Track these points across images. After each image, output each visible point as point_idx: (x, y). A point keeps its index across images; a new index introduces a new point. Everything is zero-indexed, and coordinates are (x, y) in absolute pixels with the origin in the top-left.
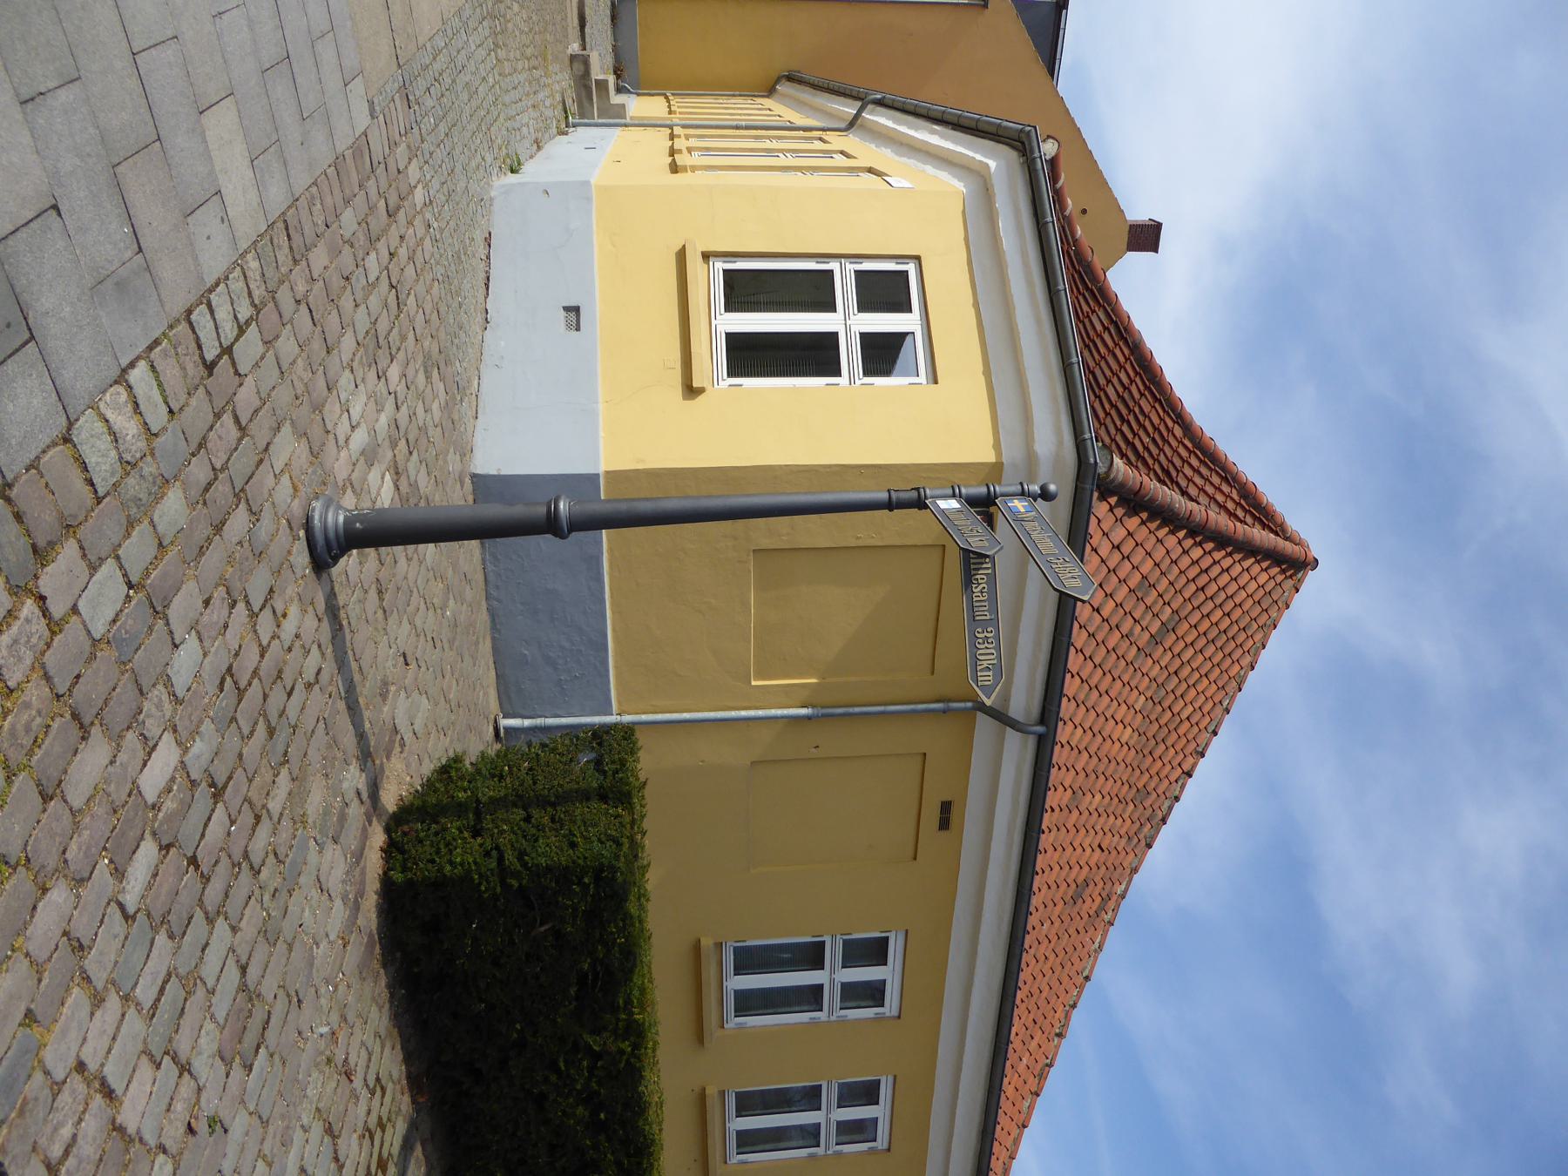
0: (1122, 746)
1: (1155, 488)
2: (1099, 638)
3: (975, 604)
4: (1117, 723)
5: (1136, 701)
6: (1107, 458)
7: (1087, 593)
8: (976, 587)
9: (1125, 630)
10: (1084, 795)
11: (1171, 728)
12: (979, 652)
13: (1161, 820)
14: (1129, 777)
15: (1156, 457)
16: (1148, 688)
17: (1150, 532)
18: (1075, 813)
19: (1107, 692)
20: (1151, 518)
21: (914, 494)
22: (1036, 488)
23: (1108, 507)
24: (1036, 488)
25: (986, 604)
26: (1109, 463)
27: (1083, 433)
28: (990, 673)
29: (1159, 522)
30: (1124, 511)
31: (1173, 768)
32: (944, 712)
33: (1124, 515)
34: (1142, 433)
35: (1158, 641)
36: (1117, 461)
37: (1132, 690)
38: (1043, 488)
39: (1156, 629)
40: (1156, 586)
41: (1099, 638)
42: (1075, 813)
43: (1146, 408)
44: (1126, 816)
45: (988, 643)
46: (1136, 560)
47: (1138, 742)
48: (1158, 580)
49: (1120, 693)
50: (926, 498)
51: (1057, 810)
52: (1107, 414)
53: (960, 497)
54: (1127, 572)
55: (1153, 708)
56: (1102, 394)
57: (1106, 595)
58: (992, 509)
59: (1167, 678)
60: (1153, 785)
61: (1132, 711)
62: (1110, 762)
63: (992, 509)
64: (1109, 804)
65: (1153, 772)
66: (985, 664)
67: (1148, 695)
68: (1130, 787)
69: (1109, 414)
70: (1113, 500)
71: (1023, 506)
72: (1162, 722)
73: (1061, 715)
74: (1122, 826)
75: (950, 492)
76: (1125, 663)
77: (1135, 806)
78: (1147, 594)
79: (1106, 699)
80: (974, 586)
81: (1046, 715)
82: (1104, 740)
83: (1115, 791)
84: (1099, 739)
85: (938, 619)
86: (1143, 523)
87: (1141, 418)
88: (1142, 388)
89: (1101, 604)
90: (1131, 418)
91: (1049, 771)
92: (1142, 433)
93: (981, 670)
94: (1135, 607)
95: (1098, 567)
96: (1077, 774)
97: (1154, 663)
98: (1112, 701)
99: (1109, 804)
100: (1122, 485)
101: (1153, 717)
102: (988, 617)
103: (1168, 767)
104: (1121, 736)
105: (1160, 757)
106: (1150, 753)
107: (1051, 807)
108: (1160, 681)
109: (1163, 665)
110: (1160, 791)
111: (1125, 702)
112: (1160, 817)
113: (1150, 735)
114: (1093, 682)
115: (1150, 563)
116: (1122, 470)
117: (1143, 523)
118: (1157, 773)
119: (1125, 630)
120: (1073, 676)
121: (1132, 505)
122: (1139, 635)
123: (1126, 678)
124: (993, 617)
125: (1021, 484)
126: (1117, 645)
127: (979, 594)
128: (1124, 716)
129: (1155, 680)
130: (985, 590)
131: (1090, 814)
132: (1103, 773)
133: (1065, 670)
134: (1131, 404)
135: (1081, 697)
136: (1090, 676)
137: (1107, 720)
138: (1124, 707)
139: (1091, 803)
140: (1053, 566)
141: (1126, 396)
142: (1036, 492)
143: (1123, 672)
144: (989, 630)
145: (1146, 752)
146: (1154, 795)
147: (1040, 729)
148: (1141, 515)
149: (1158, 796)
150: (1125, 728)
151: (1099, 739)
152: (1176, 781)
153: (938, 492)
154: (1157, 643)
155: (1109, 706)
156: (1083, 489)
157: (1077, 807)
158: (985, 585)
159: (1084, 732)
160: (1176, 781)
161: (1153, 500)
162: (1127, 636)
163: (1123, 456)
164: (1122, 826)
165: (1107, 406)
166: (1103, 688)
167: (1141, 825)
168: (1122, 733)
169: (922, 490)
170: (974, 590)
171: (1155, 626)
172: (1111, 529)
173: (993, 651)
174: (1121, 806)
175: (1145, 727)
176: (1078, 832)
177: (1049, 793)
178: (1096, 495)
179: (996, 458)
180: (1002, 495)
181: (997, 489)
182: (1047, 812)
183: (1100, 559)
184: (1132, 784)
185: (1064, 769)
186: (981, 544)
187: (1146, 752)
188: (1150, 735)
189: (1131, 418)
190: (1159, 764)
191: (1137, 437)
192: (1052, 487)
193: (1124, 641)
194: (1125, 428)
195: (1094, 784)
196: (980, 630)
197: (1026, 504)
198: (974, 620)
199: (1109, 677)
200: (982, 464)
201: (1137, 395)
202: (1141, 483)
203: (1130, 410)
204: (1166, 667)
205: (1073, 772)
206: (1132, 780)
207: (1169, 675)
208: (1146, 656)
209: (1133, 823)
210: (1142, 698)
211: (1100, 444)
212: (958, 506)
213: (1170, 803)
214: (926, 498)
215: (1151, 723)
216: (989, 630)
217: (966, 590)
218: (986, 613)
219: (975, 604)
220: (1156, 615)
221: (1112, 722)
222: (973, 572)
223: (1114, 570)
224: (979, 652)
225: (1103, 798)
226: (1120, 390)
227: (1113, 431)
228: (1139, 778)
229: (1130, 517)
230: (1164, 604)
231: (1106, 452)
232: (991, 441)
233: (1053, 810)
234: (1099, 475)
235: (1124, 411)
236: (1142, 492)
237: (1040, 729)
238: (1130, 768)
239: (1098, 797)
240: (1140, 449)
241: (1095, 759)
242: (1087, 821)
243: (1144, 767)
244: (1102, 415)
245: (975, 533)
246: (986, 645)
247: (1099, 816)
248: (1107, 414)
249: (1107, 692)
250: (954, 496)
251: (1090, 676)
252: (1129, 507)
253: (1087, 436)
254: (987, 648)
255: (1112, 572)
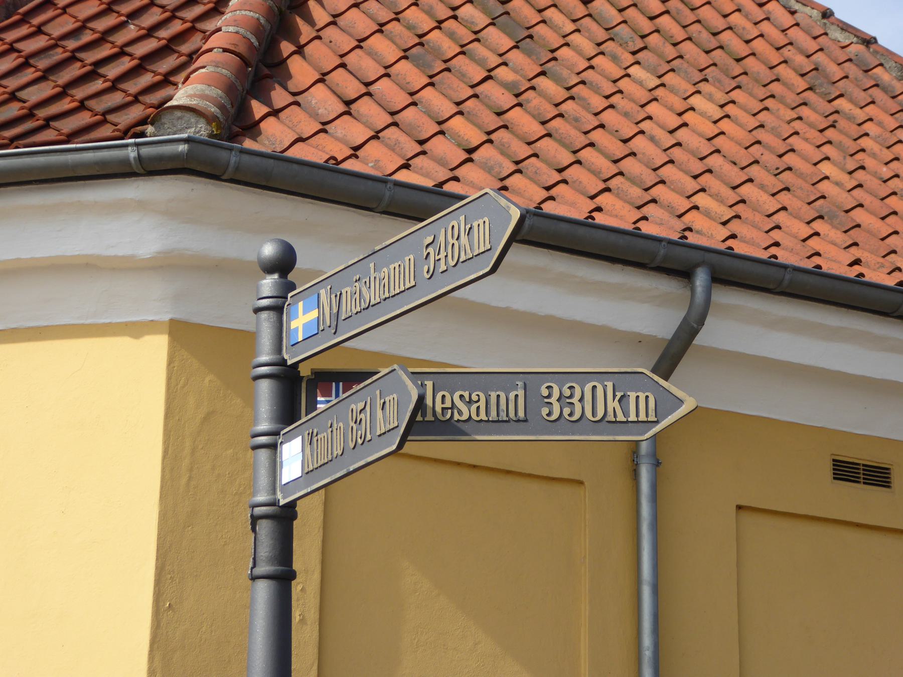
0: (728, 116)
1: (235, 23)
2: (525, 151)
3: (493, 415)
4: (685, 125)
5: (640, 83)
6: (179, 118)
7: (506, 210)
8: (460, 413)
9: (506, 100)
10: (823, 197)
11: (691, 17)
12: (589, 414)
13: (867, 46)
14: (786, 105)
15: (167, 14)
16: (615, 59)
17: (319, 38)
18: (859, 215)
19: (625, 141)
20: (292, 34)
21: (264, 527)
22: (269, 283)
23: (271, 120)
24: (269, 283)
25: (493, 395)
26: (188, 116)
27: (126, 162)
28: (632, 395)
29: (298, 20)
30: (277, 86)
31: (768, 19)
32: (657, 464)
33: (286, 89)
34: (121, 38)
35: (526, 33)
36: (182, 96)
37: (620, 92)
38: (269, 268)
39: (482, 16)
40: (420, 32)
41: (523, 151)
42: (859, 215)
43: (66, 24)
44: (861, 115)
45: (571, 396)
46: (372, 70)
47: (718, 83)
48: (409, 27)
49: (626, 115)
50: (274, 503)
51: (855, 253)
52: (82, 106)
53: (276, 433)
54: (395, 87)
55: (654, 51)
56: (43, 113)
57: (442, 132)
58: (305, 371)
59: (595, 20)
60: (799, 59)
61: (660, 92)
62: (759, 142)
63: (305, 371)
64: (840, 147)
65: (775, 58)
66: (613, 404)
67: (630, 59)
68: (805, 104)
69: (82, 102)
70: (258, 109)
71: (304, 313)
72: (679, 34)
73: (675, 237)
74: (880, 124)
75: (263, 454)
76: (570, 102)
77: (841, 96)
78: (436, 52)
79: (639, 143)
80: (456, 417)
81: (675, 267)
82: (718, 151)
83: (813, 134)
84: (715, 161)
85: (474, 467)
86: (300, 50)
87: (87, 37)
88: (24, 30)
89: (459, 145)
90: (92, 57)
91: (785, 267)
92: (121, 38)
93: (626, 414)
94: (462, 76)
95: (387, 146)
96: (784, 208)
97: (567, 44)
98: (642, 132)
99: (840, 147)
100: (230, 89)
101: (671, 52)
102: (521, 393)
103: (765, 27)
104: (709, 118)
105: (748, 42)
106: (738, 60)
107: (851, 265)
108: (602, 35)
109: (570, 27)
110: (812, 46)
111: (643, 106)
112: (861, 48)
113: (704, 60)
114: (609, 169)
115: (377, 43)
116: (200, 87)
117: (300, 50)
118: (778, 49)
119: (507, 100)
120: (599, 209)
121: (266, 71)
122: (516, 71)
123: (598, 103)
124: (520, 384)
125: (257, 310)
126: (534, 116)
127: (474, 407)
128: (671, 109)
129: (599, 45)
130: (466, 395)
131: (860, 186)
132: (780, 156)
133: (588, 224)
134: (58, 55)
135: (636, 193)
136: (595, 173)
137: (679, 144)
138: (652, 109)
139: (837, 184)
140: (443, 267)
141: (43, 63)
142: (276, 284)
143: (586, 106)
144: (545, 392)
145: (737, 69)
146: (819, 57)
147: (701, 278)
148: (285, 55)
149: (821, 50)
150: (692, 109)
151: (715, 161)
152: (793, 13)
153: (263, 479)
154: (530, 37)
155: (652, 139)
156: (237, 169)
157: (847, 211)
158: (456, 397)
159: (703, 190)
160: (793, 13)
161: (258, 30)
162: (517, 96)
163: (167, 81)
164: (880, 124)
165: (65, 105)
166: (619, 150)
167: (877, 85)
168: (703, 114)
169: (258, 511)
170: (465, 417)
171: (498, 38)
172: (313, 115)
173: (588, 388)
174: (842, 123)
175: (690, 69)
176: (895, 213)
177: (825, 269)
178: (248, 144)
179: (161, 333)
180: (278, 348)
181: (264, 358)
182: (861, 275)
183: (373, 143)
184: (799, 100)
185: (776, 235)
186: (391, 409)
187: (737, 69)
188: (704, 60)
189: (92, 57)
190: (758, 45)
191: (129, 49)
192: (269, 250)
193: (528, 101)
194: (113, 71)
195: (801, 176)
196: (545, 411)
197: (301, 304)
198: (526, 421)
199: (596, 136)
200: (170, 362)
201: (40, 42)
202: (225, 50)
203: (72, 58)
204: (574, 21)
205: (781, 218)
206: (793, 99)
207: (590, 15)
208: (555, 59)
209: (873, 102)
210: (634, 71)
211: (150, 129)
212: (298, 442)
213: (834, 27)
214: (274, 503)
215: (681, 57)
216: (545, 392)
217: (466, 434)
218: (512, 396)
219: (493, 415)
220: (477, 36)
221: (682, 134)
222: (429, 417)
223: (393, 114)
224: (589, 414)
225: (827, 158)
226: (29, 75)
227: (117, 98)
228: (788, 86)
229: (289, 76)
230: (455, 17)
231: (166, 119)
232: (124, 342)
233: (857, 262)
234: (211, 136)
235: (74, 71)
236: (242, 49)
237: (701, 278)
238: (769, 103)
239: (826, 168)
240: (150, 45)
241: (754, 171)
242: (805, 159)
243: (766, 75)
244: (84, 118)
245: (365, 417)
246: (575, 400)
247: (863, 168)
248: (82, 106)
249: (625, 141)
250: (273, 447)
251: (595, 173)
252: (270, 77)
253: (132, 153)
254: (581, 400)
255: (397, 118)
